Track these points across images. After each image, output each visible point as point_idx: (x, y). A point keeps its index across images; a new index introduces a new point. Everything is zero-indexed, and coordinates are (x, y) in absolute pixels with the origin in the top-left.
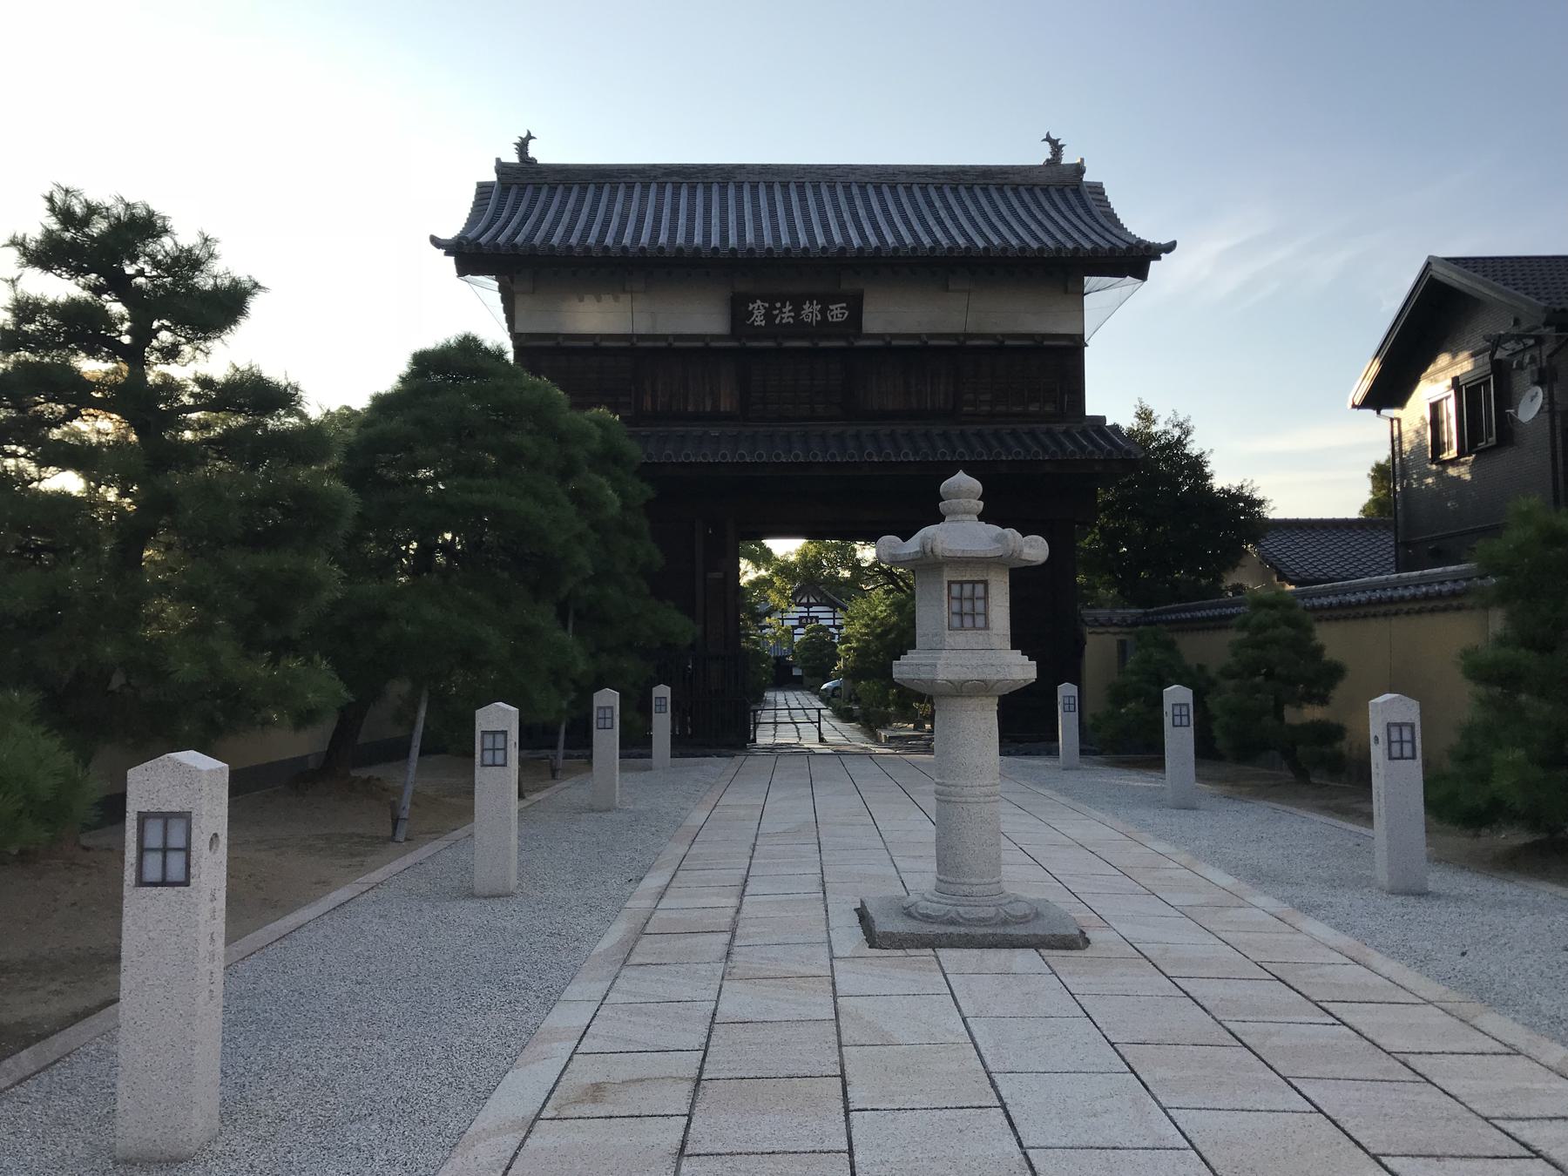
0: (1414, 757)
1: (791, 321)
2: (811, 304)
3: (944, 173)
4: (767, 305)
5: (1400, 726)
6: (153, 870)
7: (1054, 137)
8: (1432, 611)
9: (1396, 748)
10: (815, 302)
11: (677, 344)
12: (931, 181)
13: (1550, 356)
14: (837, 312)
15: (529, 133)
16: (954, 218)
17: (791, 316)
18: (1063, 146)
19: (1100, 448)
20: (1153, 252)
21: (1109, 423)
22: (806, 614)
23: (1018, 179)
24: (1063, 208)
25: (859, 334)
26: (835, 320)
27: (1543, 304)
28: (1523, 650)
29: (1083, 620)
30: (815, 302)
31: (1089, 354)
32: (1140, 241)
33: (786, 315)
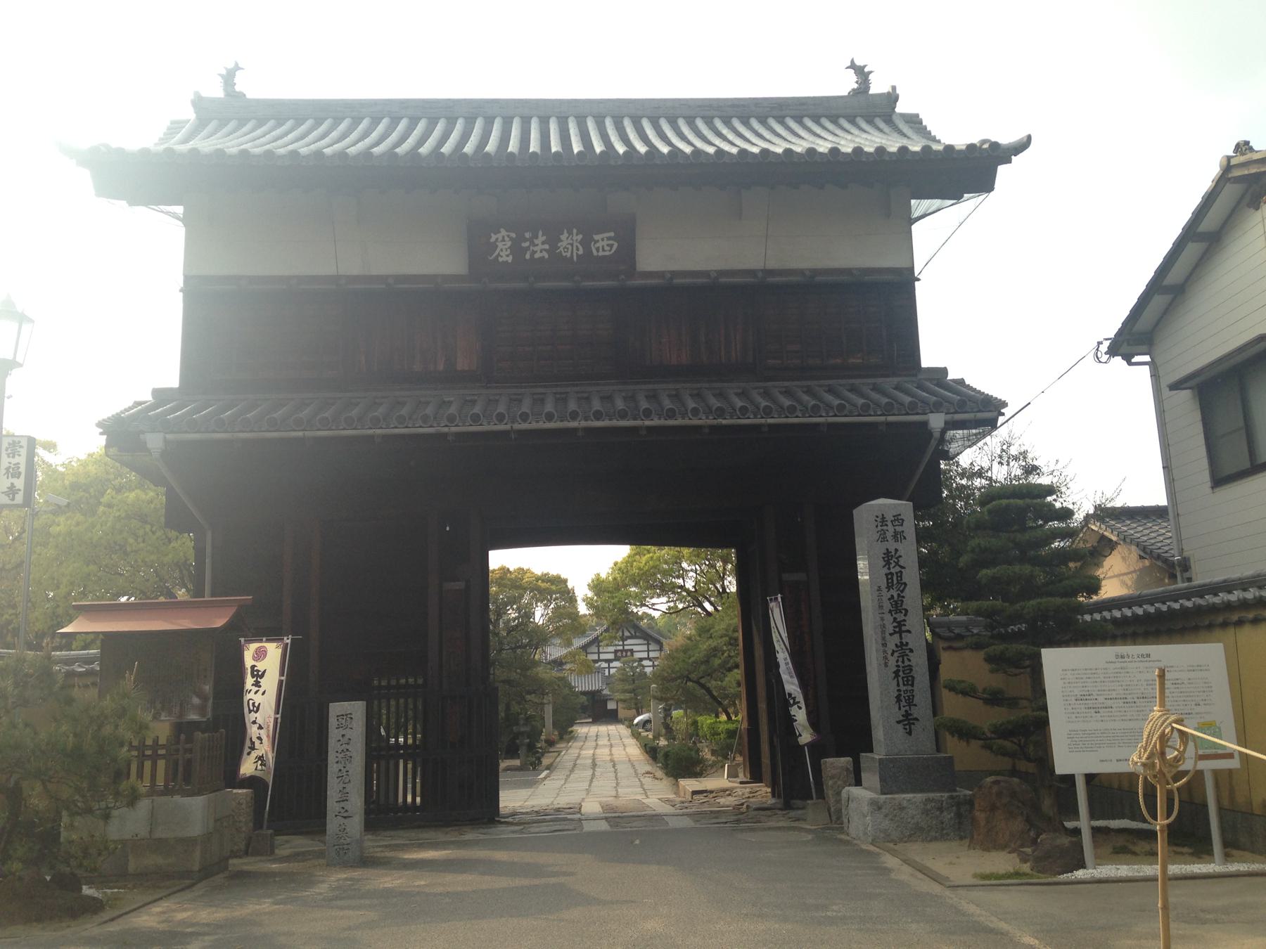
2: (570, 233)
4: (513, 235)
7: (858, 63)
10: (575, 231)
15: (237, 64)
17: (545, 250)
18: (870, 72)
21: (952, 376)
22: (621, 648)
25: (631, 270)
26: (601, 253)
30: (575, 231)
31: (924, 294)
33: (540, 249)
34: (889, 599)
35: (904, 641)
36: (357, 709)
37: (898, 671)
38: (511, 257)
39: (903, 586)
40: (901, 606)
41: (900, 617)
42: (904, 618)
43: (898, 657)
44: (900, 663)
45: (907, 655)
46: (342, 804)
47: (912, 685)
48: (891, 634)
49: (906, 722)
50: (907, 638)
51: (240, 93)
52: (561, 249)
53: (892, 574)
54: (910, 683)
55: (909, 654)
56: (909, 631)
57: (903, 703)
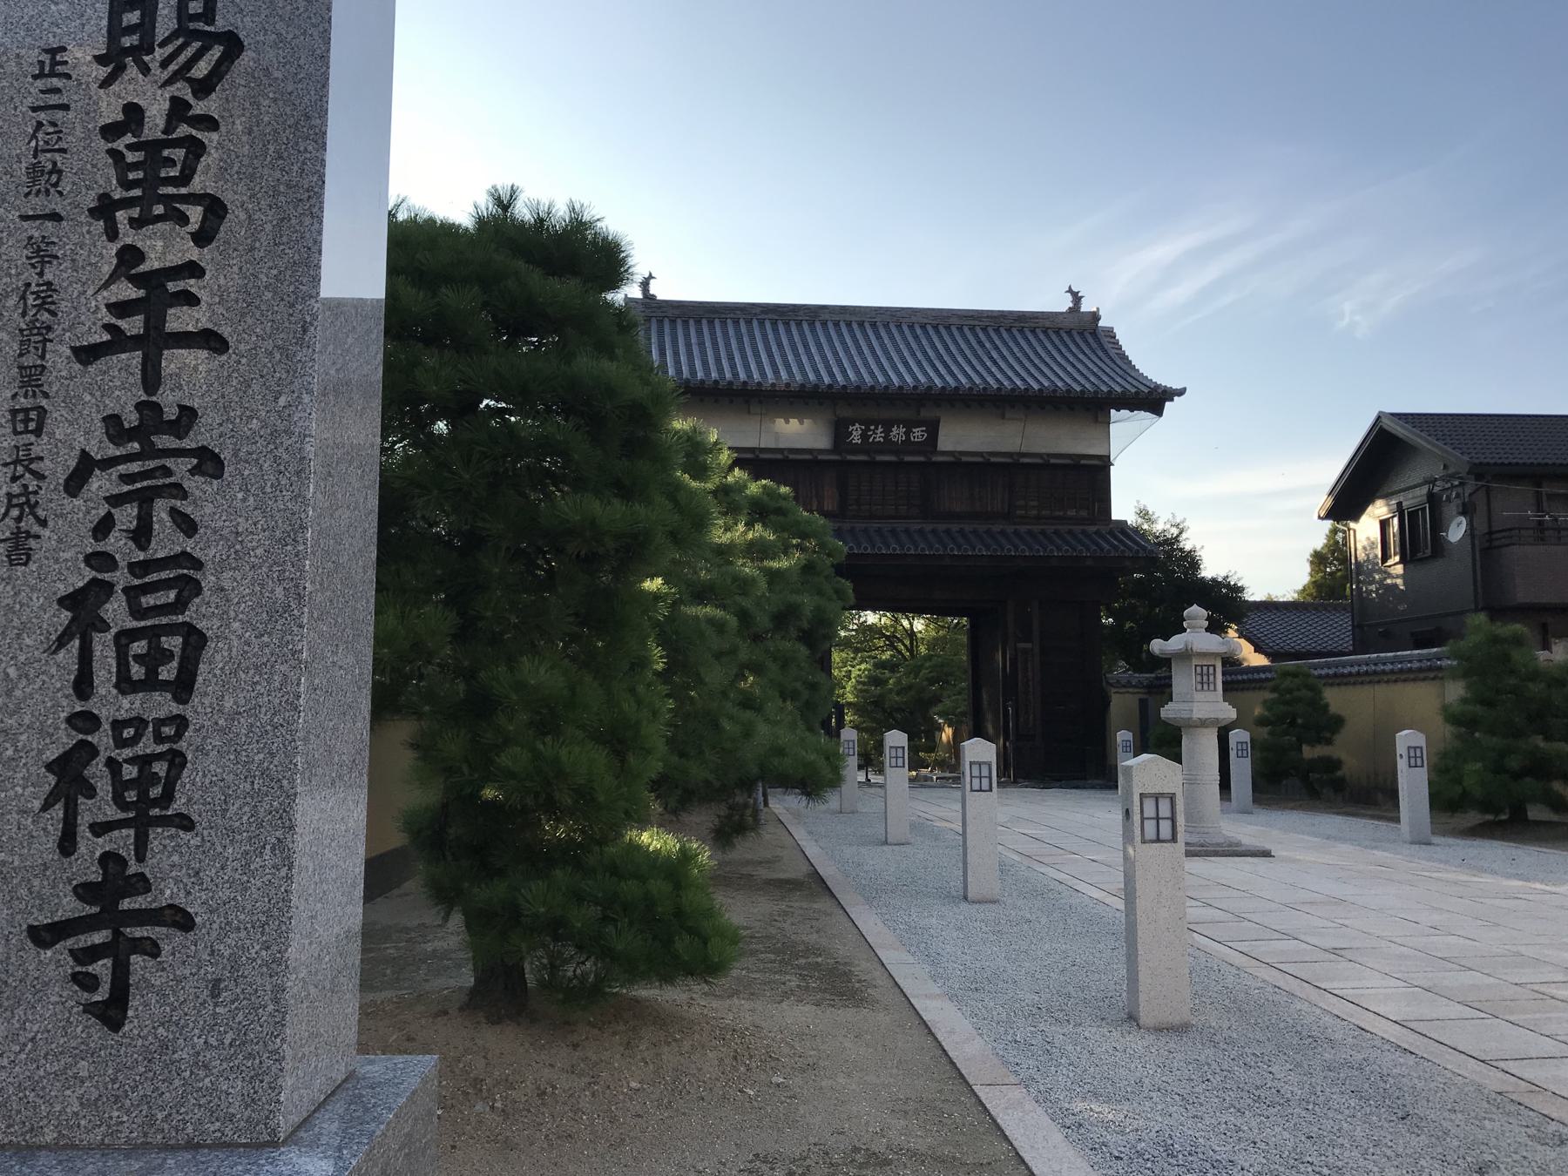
0: (1422, 766)
1: (882, 440)
2: (898, 427)
3: (988, 317)
5: (1415, 748)
6: (1244, 745)
7: (1075, 290)
8: (1405, 680)
9: (1413, 761)
11: (791, 456)
12: (976, 323)
13: (1470, 495)
14: (918, 434)
15: (650, 274)
16: (1004, 358)
18: (1082, 297)
19: (1130, 549)
20: (1167, 395)
23: (1048, 324)
24: (1088, 351)
27: (1466, 458)
28: (1478, 706)
29: (1108, 683)
32: (1158, 386)
33: (878, 436)
34: (110, 132)
35: (169, 400)
37: (100, 590)
39: (216, 52)
40: (185, 178)
42: (194, 254)
43: (116, 500)
44: (118, 544)
45: (179, 491)
47: (183, 687)
48: (87, 354)
49: (99, 937)
51: (653, 295)
54: (167, 672)
55: (193, 484)
57: (101, 806)
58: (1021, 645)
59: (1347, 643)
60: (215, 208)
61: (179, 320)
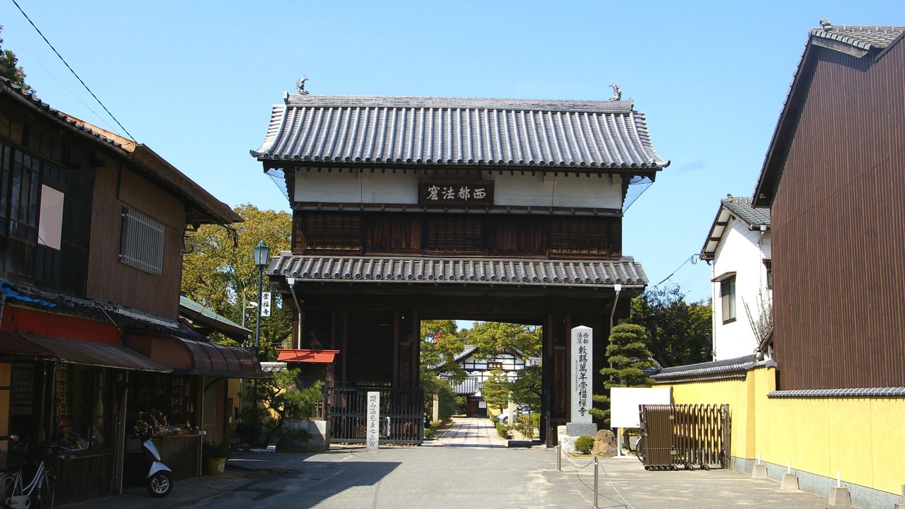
1: (453, 197)
2: (464, 188)
4: (439, 189)
10: (466, 188)
14: (479, 194)
26: (478, 197)
30: (466, 188)
31: (625, 221)
33: (450, 194)
36: (377, 394)
38: (437, 198)
41: (583, 372)
46: (372, 428)
50: (585, 380)
52: (460, 195)
53: (582, 356)
56: (586, 378)
57: (582, 404)
58: (556, 348)
59: (507, 445)
60: (586, 370)
61: (584, 377)
